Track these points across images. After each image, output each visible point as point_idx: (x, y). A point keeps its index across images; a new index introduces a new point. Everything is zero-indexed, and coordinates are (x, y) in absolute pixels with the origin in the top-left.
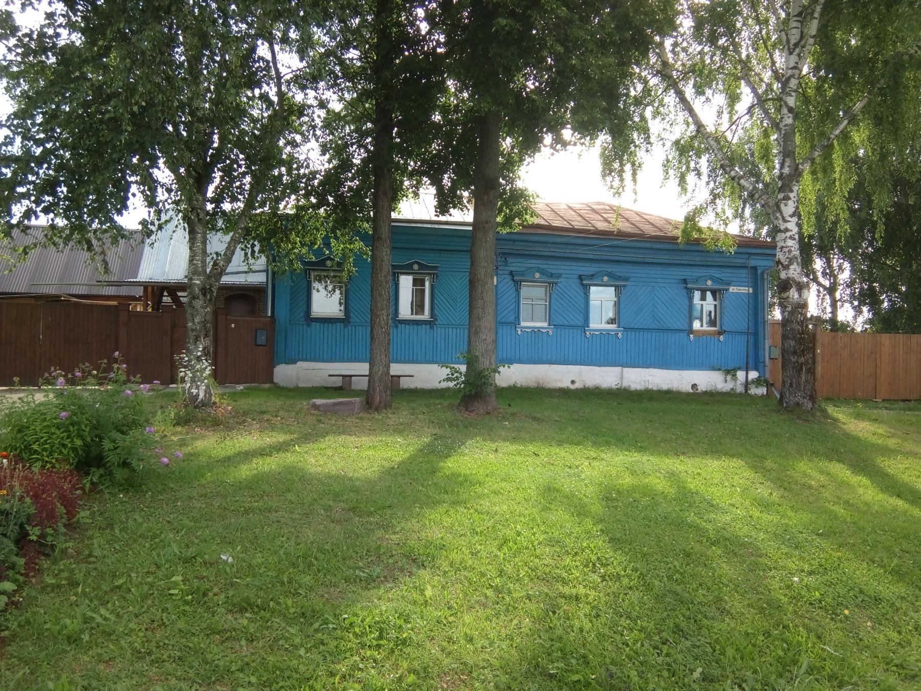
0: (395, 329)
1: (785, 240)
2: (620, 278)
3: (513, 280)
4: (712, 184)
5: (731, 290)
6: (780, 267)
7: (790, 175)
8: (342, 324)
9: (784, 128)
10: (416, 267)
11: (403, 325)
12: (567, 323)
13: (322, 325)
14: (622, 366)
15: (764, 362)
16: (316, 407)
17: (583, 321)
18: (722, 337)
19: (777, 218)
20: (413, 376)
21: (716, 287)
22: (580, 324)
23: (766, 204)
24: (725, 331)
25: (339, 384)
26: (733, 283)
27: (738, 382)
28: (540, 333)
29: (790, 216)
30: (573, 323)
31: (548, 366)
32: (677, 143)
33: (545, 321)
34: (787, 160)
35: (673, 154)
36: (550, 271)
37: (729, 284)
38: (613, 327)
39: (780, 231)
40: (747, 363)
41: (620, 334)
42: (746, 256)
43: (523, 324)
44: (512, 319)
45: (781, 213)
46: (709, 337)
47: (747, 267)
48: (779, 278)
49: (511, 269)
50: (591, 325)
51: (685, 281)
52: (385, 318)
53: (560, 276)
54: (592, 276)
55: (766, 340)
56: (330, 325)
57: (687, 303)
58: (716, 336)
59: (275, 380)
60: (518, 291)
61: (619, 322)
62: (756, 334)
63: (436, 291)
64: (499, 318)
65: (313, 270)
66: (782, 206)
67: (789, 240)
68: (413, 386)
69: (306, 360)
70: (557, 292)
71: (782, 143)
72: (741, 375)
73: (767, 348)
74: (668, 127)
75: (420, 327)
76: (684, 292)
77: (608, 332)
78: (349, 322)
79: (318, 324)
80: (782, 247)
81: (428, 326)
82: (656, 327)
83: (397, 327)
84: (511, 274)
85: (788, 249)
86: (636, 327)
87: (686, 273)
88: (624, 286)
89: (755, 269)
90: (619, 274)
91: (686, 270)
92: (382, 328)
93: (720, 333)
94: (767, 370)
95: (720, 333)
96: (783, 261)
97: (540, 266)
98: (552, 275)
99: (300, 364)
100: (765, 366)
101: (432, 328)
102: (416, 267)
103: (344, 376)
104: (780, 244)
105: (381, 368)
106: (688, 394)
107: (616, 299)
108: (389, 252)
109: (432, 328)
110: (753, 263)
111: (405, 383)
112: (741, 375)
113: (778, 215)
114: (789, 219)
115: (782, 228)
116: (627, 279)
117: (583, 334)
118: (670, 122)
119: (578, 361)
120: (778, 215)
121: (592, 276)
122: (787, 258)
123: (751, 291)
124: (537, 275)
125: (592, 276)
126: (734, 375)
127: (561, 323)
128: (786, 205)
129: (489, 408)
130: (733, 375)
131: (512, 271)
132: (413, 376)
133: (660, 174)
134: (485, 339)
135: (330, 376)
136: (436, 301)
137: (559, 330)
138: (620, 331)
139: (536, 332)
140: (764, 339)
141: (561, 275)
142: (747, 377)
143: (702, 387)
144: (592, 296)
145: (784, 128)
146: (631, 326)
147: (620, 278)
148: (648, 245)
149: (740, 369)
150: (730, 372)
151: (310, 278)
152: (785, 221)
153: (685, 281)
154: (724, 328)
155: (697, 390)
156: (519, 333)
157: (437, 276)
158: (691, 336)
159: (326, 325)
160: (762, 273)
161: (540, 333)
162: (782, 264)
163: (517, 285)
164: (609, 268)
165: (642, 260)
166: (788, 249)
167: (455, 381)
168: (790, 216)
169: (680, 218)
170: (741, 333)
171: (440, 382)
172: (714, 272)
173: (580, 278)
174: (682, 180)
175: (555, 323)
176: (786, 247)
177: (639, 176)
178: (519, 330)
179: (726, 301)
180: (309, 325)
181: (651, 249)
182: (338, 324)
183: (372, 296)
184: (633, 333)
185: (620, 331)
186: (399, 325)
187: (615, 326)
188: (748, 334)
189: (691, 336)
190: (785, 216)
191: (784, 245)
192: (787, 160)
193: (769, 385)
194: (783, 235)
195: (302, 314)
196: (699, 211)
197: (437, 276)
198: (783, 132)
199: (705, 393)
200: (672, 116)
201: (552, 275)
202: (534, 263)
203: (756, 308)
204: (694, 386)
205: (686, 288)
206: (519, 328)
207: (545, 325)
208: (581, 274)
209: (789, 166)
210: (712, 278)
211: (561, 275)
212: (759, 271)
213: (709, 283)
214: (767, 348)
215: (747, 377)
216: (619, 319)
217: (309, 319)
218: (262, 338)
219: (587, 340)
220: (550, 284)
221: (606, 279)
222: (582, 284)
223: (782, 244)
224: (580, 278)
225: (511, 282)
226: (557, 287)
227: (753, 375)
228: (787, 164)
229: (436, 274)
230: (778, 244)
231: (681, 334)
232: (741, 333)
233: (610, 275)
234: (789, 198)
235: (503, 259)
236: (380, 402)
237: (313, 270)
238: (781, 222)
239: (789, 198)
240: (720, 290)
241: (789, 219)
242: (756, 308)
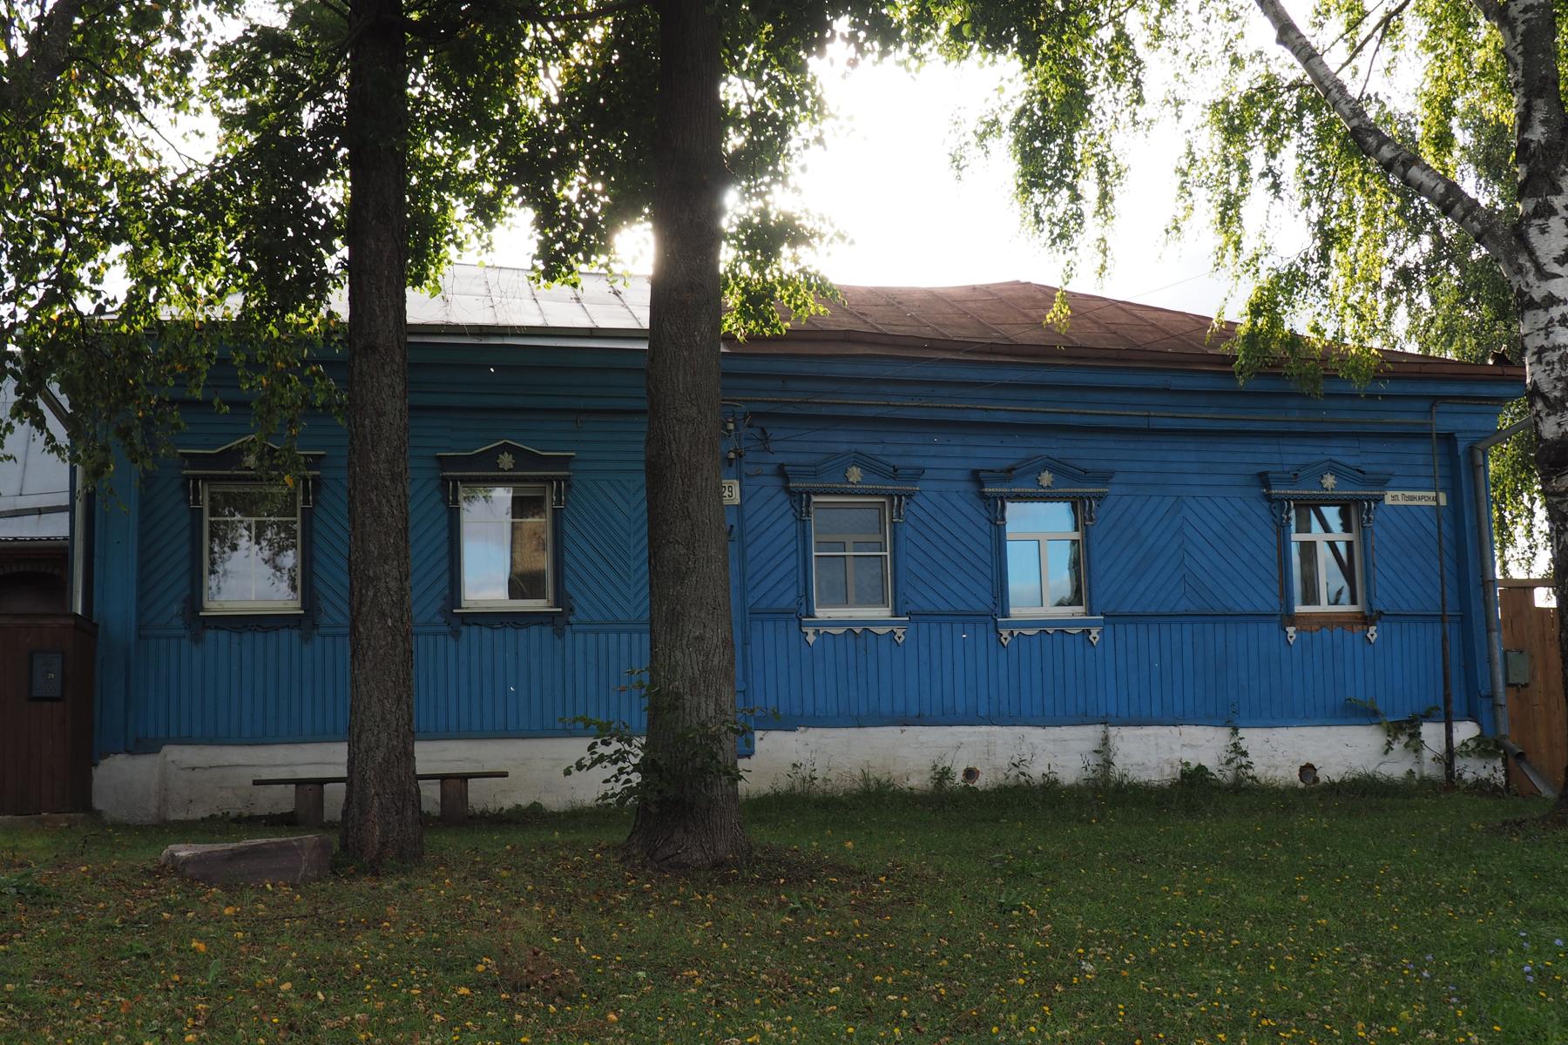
0: (451, 641)
1: (1547, 330)
2: (1085, 476)
3: (787, 490)
4: (1316, 210)
5: (1388, 500)
6: (1539, 405)
7: (1548, 147)
8: (296, 633)
9: (1522, 17)
10: (506, 460)
11: (474, 629)
12: (944, 607)
13: (235, 637)
14: (1106, 722)
15: (1492, 695)
16: (177, 868)
17: (989, 600)
18: (1372, 629)
19: (1520, 270)
20: (504, 775)
21: (1348, 492)
22: (980, 607)
23: (1485, 231)
24: (1381, 613)
25: (287, 807)
26: (1393, 483)
27: (1427, 755)
28: (870, 637)
29: (1556, 260)
30: (962, 607)
31: (897, 729)
32: (1219, 108)
33: (883, 603)
34: (1539, 103)
35: (1209, 142)
36: (893, 461)
37: (1383, 482)
38: (1078, 611)
39: (1531, 305)
40: (1447, 701)
41: (1094, 632)
42: (1425, 405)
43: (821, 613)
44: (788, 599)
45: (1531, 253)
46: (1338, 632)
47: (1427, 436)
48: (1540, 438)
49: (779, 458)
50: (1012, 611)
51: (1264, 479)
52: (393, 585)
53: (918, 474)
54: (1010, 470)
55: (1495, 634)
56: (259, 637)
57: (1274, 539)
58: (1358, 629)
59: (98, 804)
60: (802, 520)
61: (1090, 600)
62: (1464, 619)
63: (567, 528)
64: (750, 601)
65: (205, 478)
66: (1533, 233)
67: (1558, 329)
68: (508, 803)
69: (188, 740)
70: (911, 519)
71: (1520, 60)
72: (1431, 733)
73: (1498, 655)
74: (1186, 71)
75: (522, 632)
76: (1262, 510)
77: (1061, 627)
78: (315, 626)
79: (223, 635)
80: (1541, 351)
81: (548, 630)
82: (1193, 609)
83: (456, 634)
84: (782, 472)
85: (1558, 353)
86: (1137, 610)
87: (1265, 456)
88: (1100, 497)
89: (1449, 439)
90: (1084, 465)
91: (1265, 448)
92: (383, 615)
93: (1366, 620)
94: (1503, 717)
95: (1366, 620)
96: (1545, 387)
97: (863, 448)
98: (895, 473)
99: (177, 754)
100: (1495, 706)
101: (560, 634)
102: (506, 460)
103: (299, 783)
104: (1533, 343)
105: (384, 736)
106: (1292, 789)
107: (1077, 536)
108: (399, 389)
109: (560, 634)
110: (1444, 422)
111: (481, 795)
112: (1431, 733)
113: (1523, 260)
114: (1556, 269)
115: (1537, 295)
116: (1105, 477)
117: (992, 635)
118: (1192, 60)
119: (983, 712)
120: (1523, 260)
121: (1008, 474)
122: (1559, 379)
123: (1443, 501)
124: (855, 474)
125: (1008, 474)
126: (1415, 735)
127: (928, 608)
128: (1543, 231)
129: (721, 847)
130: (1411, 736)
131: (781, 466)
132: (504, 775)
133: (1170, 206)
134: (701, 638)
135: (256, 783)
136: (568, 558)
137: (924, 627)
138: (1095, 624)
139: (860, 634)
140: (1489, 631)
141: (923, 470)
142: (1449, 739)
143: (1332, 769)
144: (1011, 528)
145: (1522, 17)
146: (1125, 609)
147: (1085, 476)
148: (1157, 380)
149: (1428, 716)
150: (1404, 728)
151: (196, 501)
152: (1544, 275)
153: (1264, 479)
154: (1378, 606)
155: (1316, 780)
156: (811, 638)
157: (569, 487)
158: (1291, 630)
159: (248, 636)
160: (1471, 451)
161: (871, 637)
162: (1544, 397)
163: (800, 501)
164: (1056, 448)
165: (1143, 424)
166: (1558, 353)
167: (615, 762)
168: (1556, 260)
169: (1236, 312)
170: (1425, 617)
171: (568, 772)
172: (1338, 452)
173: (976, 477)
174: (1230, 208)
175: (911, 607)
176: (1555, 348)
177: (1115, 207)
178: (810, 631)
179: (1377, 529)
180: (197, 638)
181: (1166, 391)
182: (284, 634)
183: (352, 520)
184: (1131, 628)
185: (1095, 624)
186: (464, 629)
187: (1080, 609)
188: (1442, 618)
189: (1291, 630)
190: (1543, 260)
191: (1545, 343)
192: (1539, 103)
193: (1515, 759)
194: (1542, 317)
195: (175, 608)
196: (1290, 282)
197: (569, 487)
198: (1521, 28)
199: (1334, 788)
200: (1196, 41)
201: (895, 473)
202: (842, 441)
203: (1459, 546)
204: (1307, 770)
205: (1268, 498)
206: (809, 625)
207: (883, 613)
208: (977, 465)
209: (1544, 122)
210: (1334, 468)
211: (923, 470)
212: (1462, 446)
213: (1329, 481)
214: (1498, 655)
215: (1449, 739)
216: (1089, 589)
217: (200, 623)
218: (49, 679)
219: (1003, 653)
220: (890, 496)
221: (1046, 478)
222: (983, 496)
223: (1540, 341)
224: (976, 477)
225: (782, 497)
226: (913, 507)
227: (1465, 731)
228: (1539, 115)
229: (566, 479)
230: (1527, 341)
231: (1263, 627)
232: (1425, 617)
233: (1057, 468)
234: (1552, 212)
235: (757, 433)
236: (383, 844)
237: (205, 478)
238: (1531, 278)
239: (1552, 212)
240: (1358, 501)
241: (1556, 269)
242: (1459, 546)
